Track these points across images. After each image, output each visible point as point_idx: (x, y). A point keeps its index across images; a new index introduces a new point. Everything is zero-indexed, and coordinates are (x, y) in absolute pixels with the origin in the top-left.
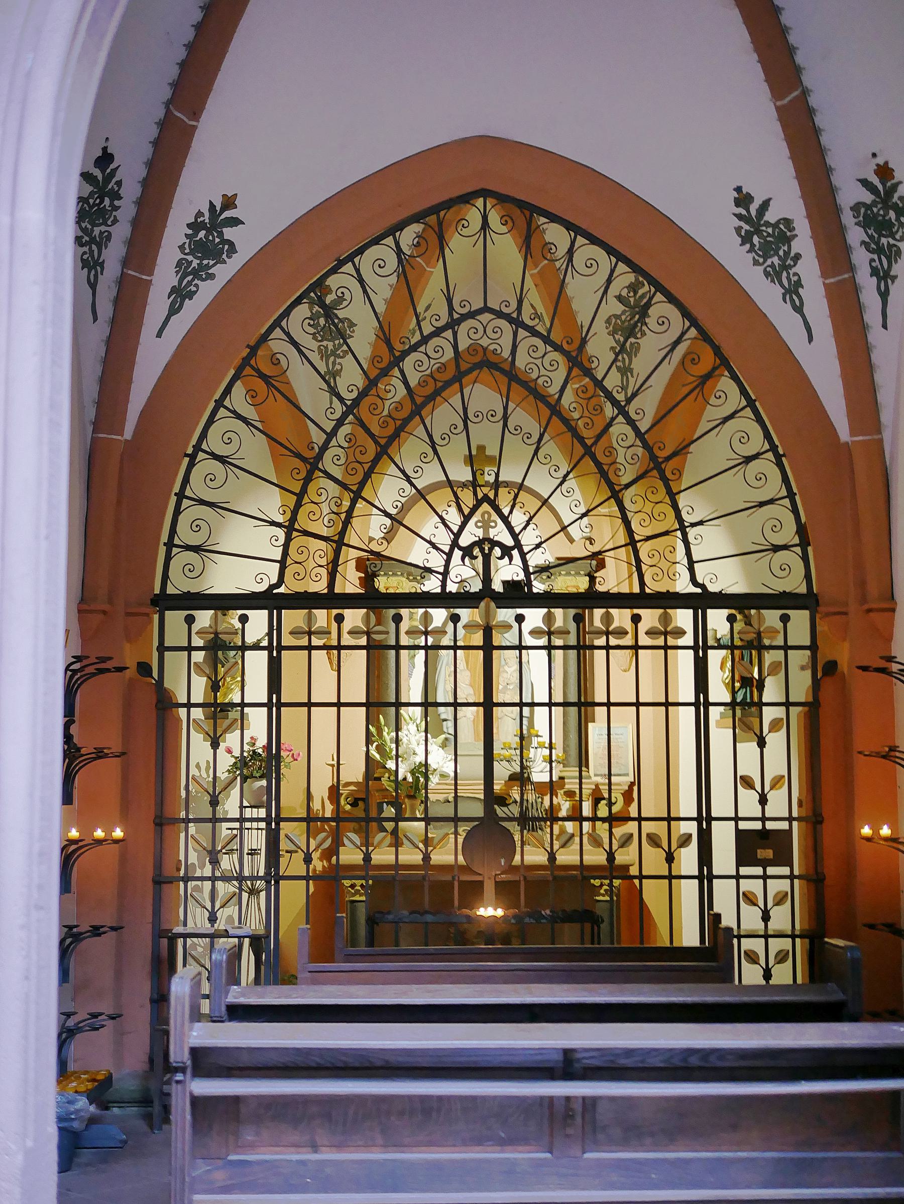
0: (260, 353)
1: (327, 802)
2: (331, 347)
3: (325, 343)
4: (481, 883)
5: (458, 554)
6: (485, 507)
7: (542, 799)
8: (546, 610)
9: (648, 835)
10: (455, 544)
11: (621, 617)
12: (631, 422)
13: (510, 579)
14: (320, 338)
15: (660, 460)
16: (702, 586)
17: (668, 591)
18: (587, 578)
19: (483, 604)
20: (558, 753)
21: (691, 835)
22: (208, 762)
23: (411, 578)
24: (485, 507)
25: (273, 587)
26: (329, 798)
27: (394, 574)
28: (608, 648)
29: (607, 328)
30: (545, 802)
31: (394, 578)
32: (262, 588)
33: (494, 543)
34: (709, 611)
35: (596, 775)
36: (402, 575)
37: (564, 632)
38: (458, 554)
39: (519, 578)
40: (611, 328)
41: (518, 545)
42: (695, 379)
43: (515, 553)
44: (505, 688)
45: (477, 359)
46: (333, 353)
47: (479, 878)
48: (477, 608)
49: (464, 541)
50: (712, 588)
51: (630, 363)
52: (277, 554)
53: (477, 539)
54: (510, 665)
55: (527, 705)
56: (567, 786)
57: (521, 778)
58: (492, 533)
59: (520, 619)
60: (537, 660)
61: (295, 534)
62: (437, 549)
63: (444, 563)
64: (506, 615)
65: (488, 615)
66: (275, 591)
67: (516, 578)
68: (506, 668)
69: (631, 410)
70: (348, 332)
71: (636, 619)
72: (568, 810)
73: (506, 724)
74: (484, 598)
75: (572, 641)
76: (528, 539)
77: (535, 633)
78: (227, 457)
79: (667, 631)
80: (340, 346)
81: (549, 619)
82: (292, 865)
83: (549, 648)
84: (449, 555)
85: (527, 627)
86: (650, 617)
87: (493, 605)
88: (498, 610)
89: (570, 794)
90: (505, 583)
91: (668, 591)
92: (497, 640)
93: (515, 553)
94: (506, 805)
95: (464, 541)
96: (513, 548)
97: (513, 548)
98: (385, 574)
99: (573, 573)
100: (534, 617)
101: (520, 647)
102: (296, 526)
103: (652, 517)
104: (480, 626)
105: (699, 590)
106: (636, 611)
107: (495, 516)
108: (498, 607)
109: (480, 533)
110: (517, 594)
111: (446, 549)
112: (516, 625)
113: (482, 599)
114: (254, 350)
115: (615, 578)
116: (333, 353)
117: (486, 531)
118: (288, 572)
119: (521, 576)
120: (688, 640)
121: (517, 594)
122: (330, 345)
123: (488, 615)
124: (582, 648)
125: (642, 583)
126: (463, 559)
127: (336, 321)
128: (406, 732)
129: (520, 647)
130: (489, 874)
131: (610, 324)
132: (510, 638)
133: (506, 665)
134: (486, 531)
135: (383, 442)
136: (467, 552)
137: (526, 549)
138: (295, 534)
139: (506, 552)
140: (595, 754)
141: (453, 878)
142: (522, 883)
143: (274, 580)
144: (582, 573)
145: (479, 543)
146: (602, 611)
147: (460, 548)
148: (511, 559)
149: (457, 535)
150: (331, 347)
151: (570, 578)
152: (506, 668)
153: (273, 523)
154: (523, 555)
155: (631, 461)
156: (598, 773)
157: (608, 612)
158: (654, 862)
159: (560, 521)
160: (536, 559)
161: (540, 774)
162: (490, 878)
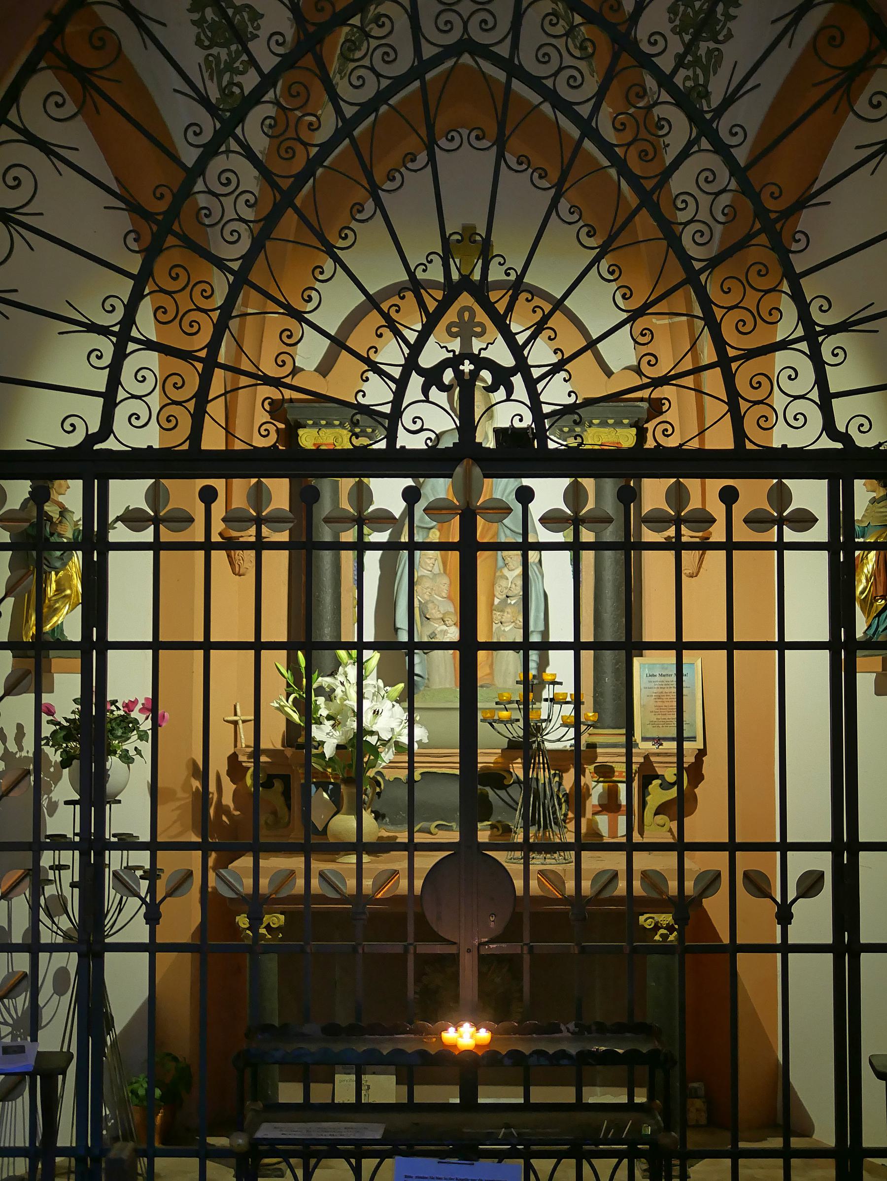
0: (69, 29)
1: (226, 780)
2: (224, 56)
3: (215, 51)
4: (454, 959)
5: (416, 381)
6: (465, 299)
7: (561, 778)
8: (567, 481)
9: (746, 875)
10: (411, 365)
11: (704, 493)
12: (722, 149)
13: (508, 425)
14: (207, 43)
15: (773, 216)
16: (845, 438)
17: (784, 446)
18: (634, 431)
19: (459, 470)
20: (588, 713)
21: (821, 875)
22: (20, 727)
23: (357, 430)
24: (465, 299)
25: (91, 439)
26: (229, 773)
27: (329, 425)
28: (677, 546)
29: (671, 21)
30: (564, 783)
31: (329, 431)
32: (75, 440)
33: (482, 363)
34: (113, 484)
35: (644, 739)
36: (342, 425)
37: (598, 520)
38: (416, 381)
39: (523, 425)
40: (677, 22)
41: (522, 366)
42: (837, 72)
43: (517, 380)
44: (504, 603)
45: (450, 39)
46: (230, 67)
47: (452, 950)
48: (449, 476)
49: (429, 358)
50: (863, 441)
51: (707, 81)
52: (100, 382)
53: (451, 355)
54: (511, 566)
55: (536, 646)
56: (599, 759)
57: (527, 744)
58: (477, 345)
59: (525, 496)
60: (555, 570)
61: (131, 346)
62: (382, 373)
63: (391, 397)
64: (503, 489)
65: (468, 490)
66: (97, 447)
67: (517, 424)
68: (505, 571)
69: (723, 127)
70: (250, 29)
71: (729, 496)
72: (600, 796)
73: (501, 673)
74: (462, 460)
75: (610, 534)
76: (541, 354)
77: (550, 520)
78: (13, 211)
79: (783, 515)
80: (238, 54)
81: (574, 496)
82: (128, 922)
83: (575, 547)
84: (402, 384)
85: (537, 509)
86: (754, 493)
87: (477, 471)
88: (485, 480)
89: (605, 772)
90: (498, 432)
91: (784, 446)
92: (484, 531)
93: (517, 380)
94: (505, 787)
95: (429, 358)
96: (512, 371)
97: (512, 371)
98: (316, 425)
99: (611, 421)
100: (550, 493)
101: (525, 547)
102: (134, 333)
103: (757, 316)
104: (455, 508)
105: (839, 446)
106: (526, 482)
107: (481, 316)
108: (486, 476)
109: (456, 345)
110: (520, 454)
111: (396, 373)
112: (518, 507)
113: (459, 461)
114: (58, 23)
115: (681, 424)
116: (230, 67)
117: (466, 343)
118: (121, 414)
119: (528, 420)
120: (820, 532)
121: (520, 454)
122: (223, 53)
123: (468, 490)
124: (630, 548)
125: (739, 434)
126: (425, 390)
127: (230, 12)
128: (342, 679)
129: (525, 547)
130: (470, 937)
131: (676, 14)
132: (508, 530)
133: (500, 576)
134: (466, 343)
135: (285, 184)
136: (432, 377)
137: (536, 373)
138: (131, 346)
139: (502, 377)
140: (643, 706)
141: (406, 949)
142: (527, 958)
143: (94, 428)
144: (626, 421)
145: (454, 362)
146: (352, 481)
147: (421, 372)
148: (510, 390)
149: (416, 349)
150: (224, 56)
151: (606, 430)
152: (505, 571)
153: (93, 328)
154: (531, 384)
155: (721, 218)
156: (648, 736)
157: (781, 485)
158: (756, 921)
159: (593, 341)
160: (556, 393)
161: (558, 737)
162: (469, 951)
